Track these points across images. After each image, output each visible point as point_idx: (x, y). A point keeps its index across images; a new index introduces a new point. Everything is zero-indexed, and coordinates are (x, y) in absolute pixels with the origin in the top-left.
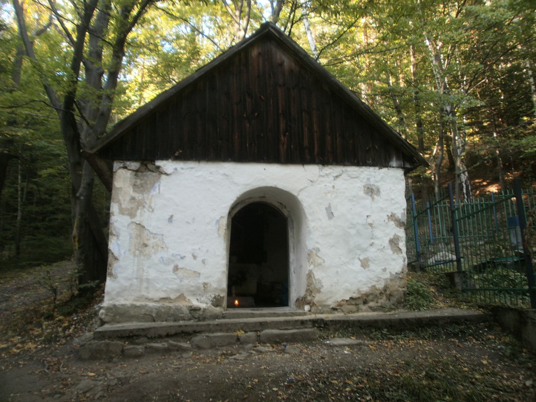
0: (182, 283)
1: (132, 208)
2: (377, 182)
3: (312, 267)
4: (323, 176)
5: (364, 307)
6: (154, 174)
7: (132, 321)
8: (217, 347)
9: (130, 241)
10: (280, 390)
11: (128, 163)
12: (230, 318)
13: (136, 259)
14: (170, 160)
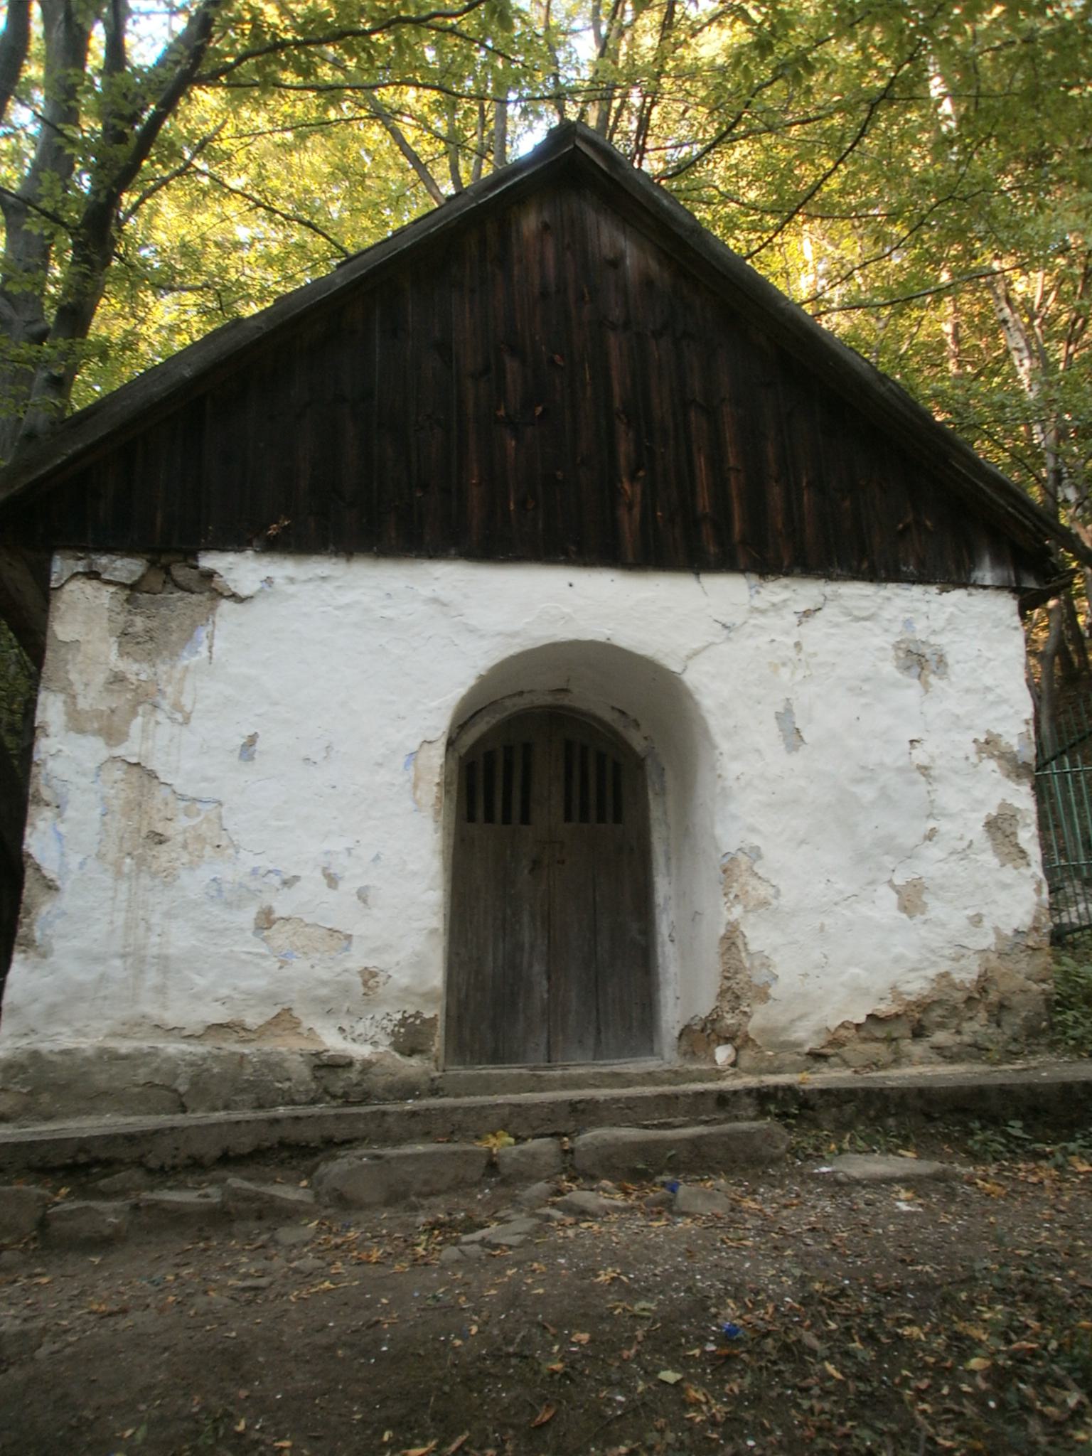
0: (286, 972)
1: (113, 711)
2: (934, 632)
3: (737, 911)
4: (762, 612)
5: (917, 1049)
6: (194, 598)
7: (100, 1112)
8: (413, 1199)
9: (104, 824)
10: (688, 1378)
11: (104, 560)
12: (458, 1096)
13: (124, 886)
14: (250, 553)
